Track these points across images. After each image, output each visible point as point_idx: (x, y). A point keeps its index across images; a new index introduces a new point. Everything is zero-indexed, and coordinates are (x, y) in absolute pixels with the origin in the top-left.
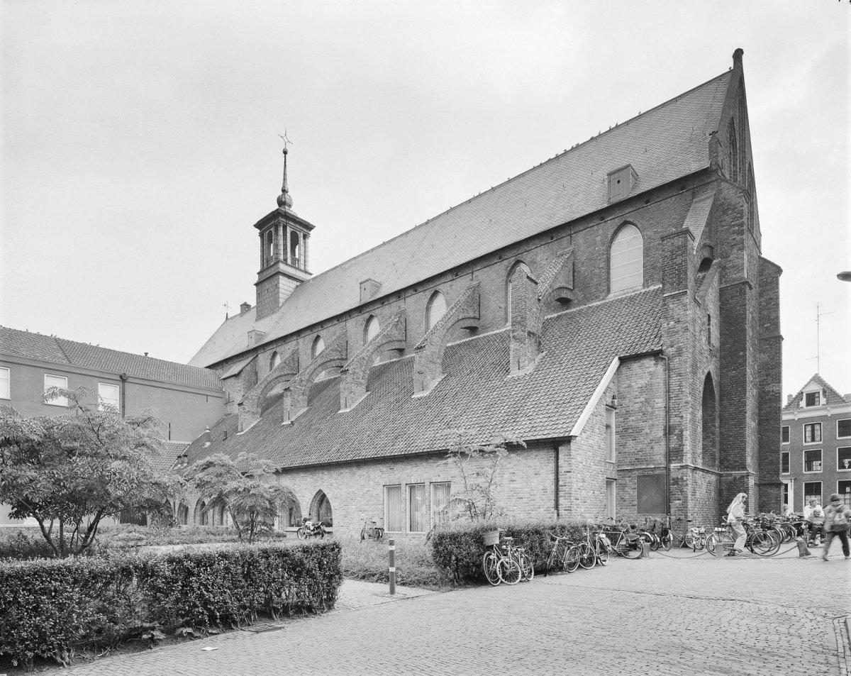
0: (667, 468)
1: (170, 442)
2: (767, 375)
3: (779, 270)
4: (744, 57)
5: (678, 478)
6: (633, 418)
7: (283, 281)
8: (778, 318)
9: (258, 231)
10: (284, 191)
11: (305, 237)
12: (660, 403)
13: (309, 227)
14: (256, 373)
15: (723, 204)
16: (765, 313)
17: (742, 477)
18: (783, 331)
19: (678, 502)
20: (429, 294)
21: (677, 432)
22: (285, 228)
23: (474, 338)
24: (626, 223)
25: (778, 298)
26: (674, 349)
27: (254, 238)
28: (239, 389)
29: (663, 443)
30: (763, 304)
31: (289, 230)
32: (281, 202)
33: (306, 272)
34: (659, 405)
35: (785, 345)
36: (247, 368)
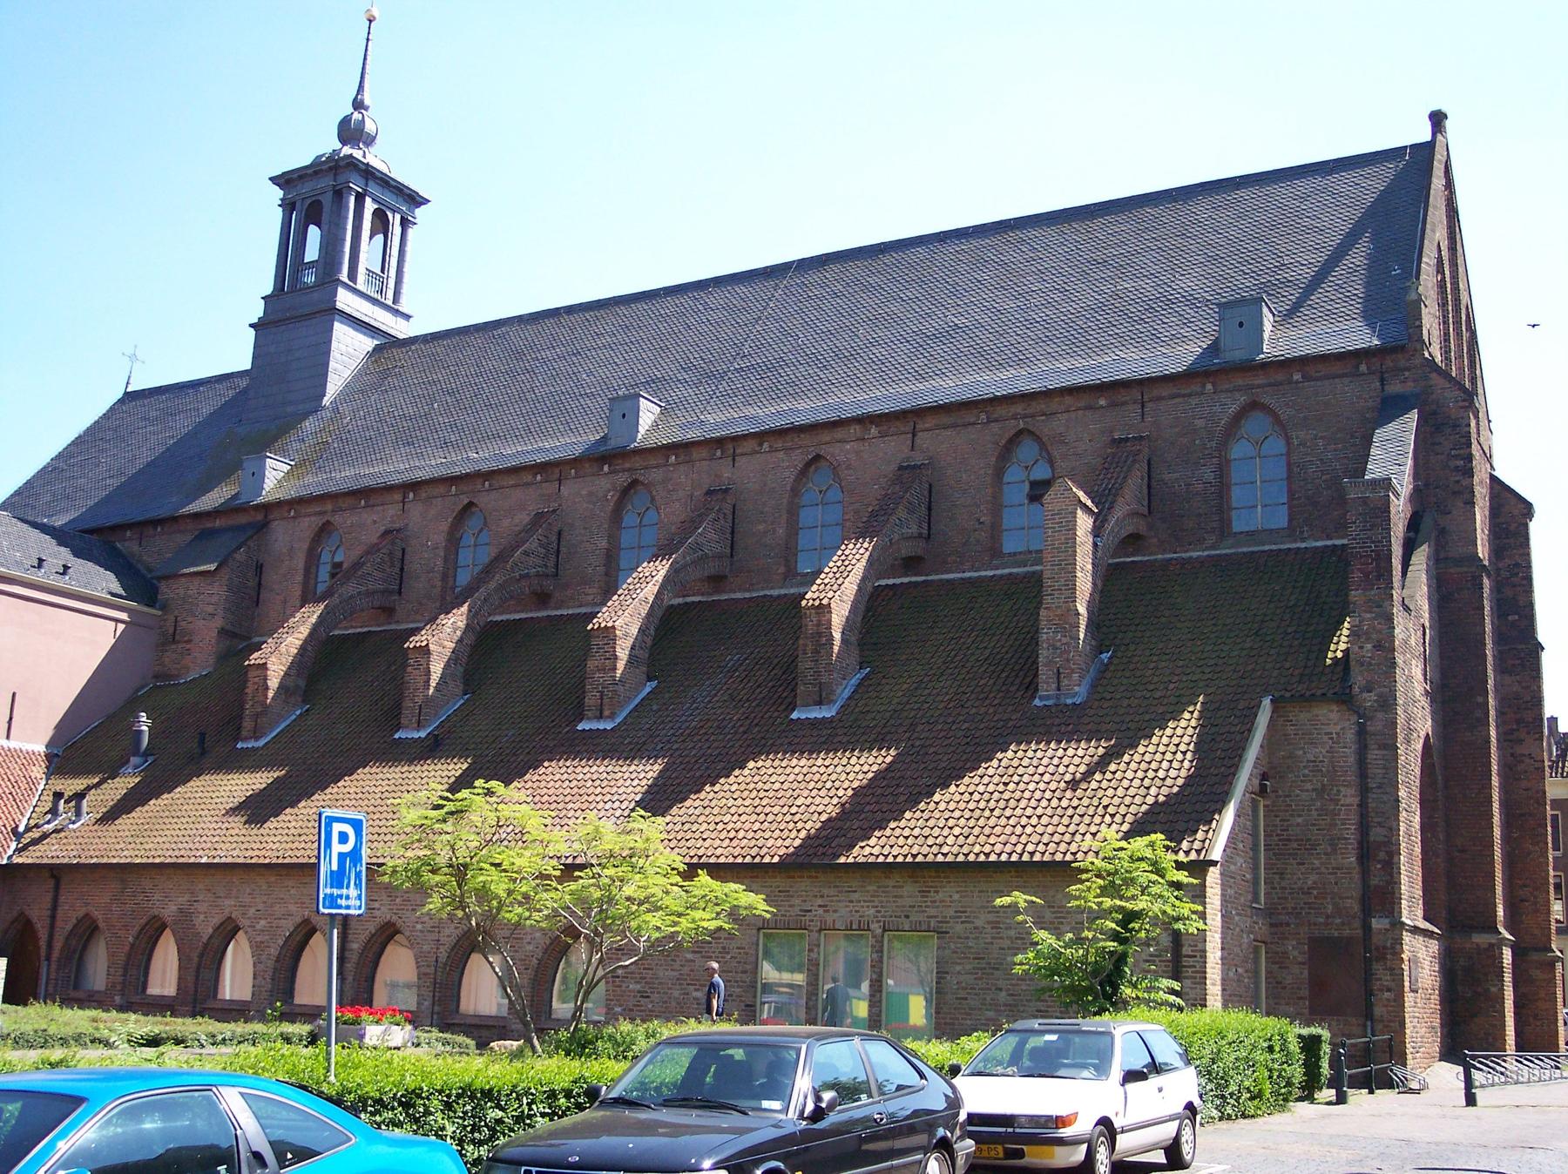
0: (1367, 928)
1: (13, 744)
2: (1518, 722)
3: (1529, 506)
4: (1448, 124)
5: (1385, 948)
6: (1300, 820)
7: (340, 330)
8: (1531, 605)
9: (281, 193)
10: (358, 105)
11: (405, 223)
12: (1349, 797)
13: (415, 200)
14: (260, 569)
15: (1435, 413)
16: (1509, 593)
17: (1491, 945)
18: (1542, 635)
19: (1387, 994)
20: (798, 459)
21: (1382, 855)
22: (360, 199)
23: (914, 579)
24: (1254, 405)
25: (1529, 567)
26: (1373, 696)
27: (266, 214)
28: (210, 609)
29: (1356, 876)
30: (1505, 574)
31: (370, 206)
32: (350, 132)
33: (397, 313)
34: (1348, 801)
35: (1546, 659)
36: (237, 556)
